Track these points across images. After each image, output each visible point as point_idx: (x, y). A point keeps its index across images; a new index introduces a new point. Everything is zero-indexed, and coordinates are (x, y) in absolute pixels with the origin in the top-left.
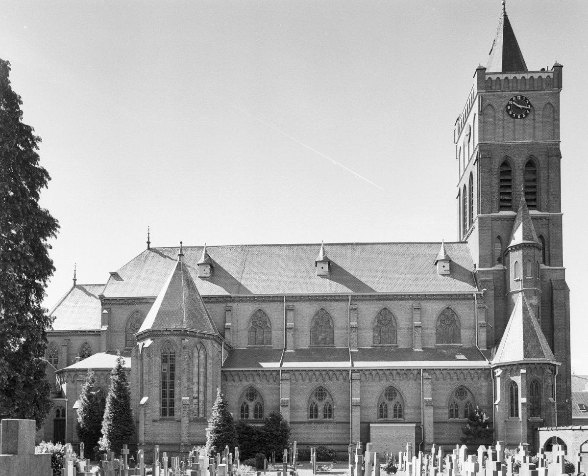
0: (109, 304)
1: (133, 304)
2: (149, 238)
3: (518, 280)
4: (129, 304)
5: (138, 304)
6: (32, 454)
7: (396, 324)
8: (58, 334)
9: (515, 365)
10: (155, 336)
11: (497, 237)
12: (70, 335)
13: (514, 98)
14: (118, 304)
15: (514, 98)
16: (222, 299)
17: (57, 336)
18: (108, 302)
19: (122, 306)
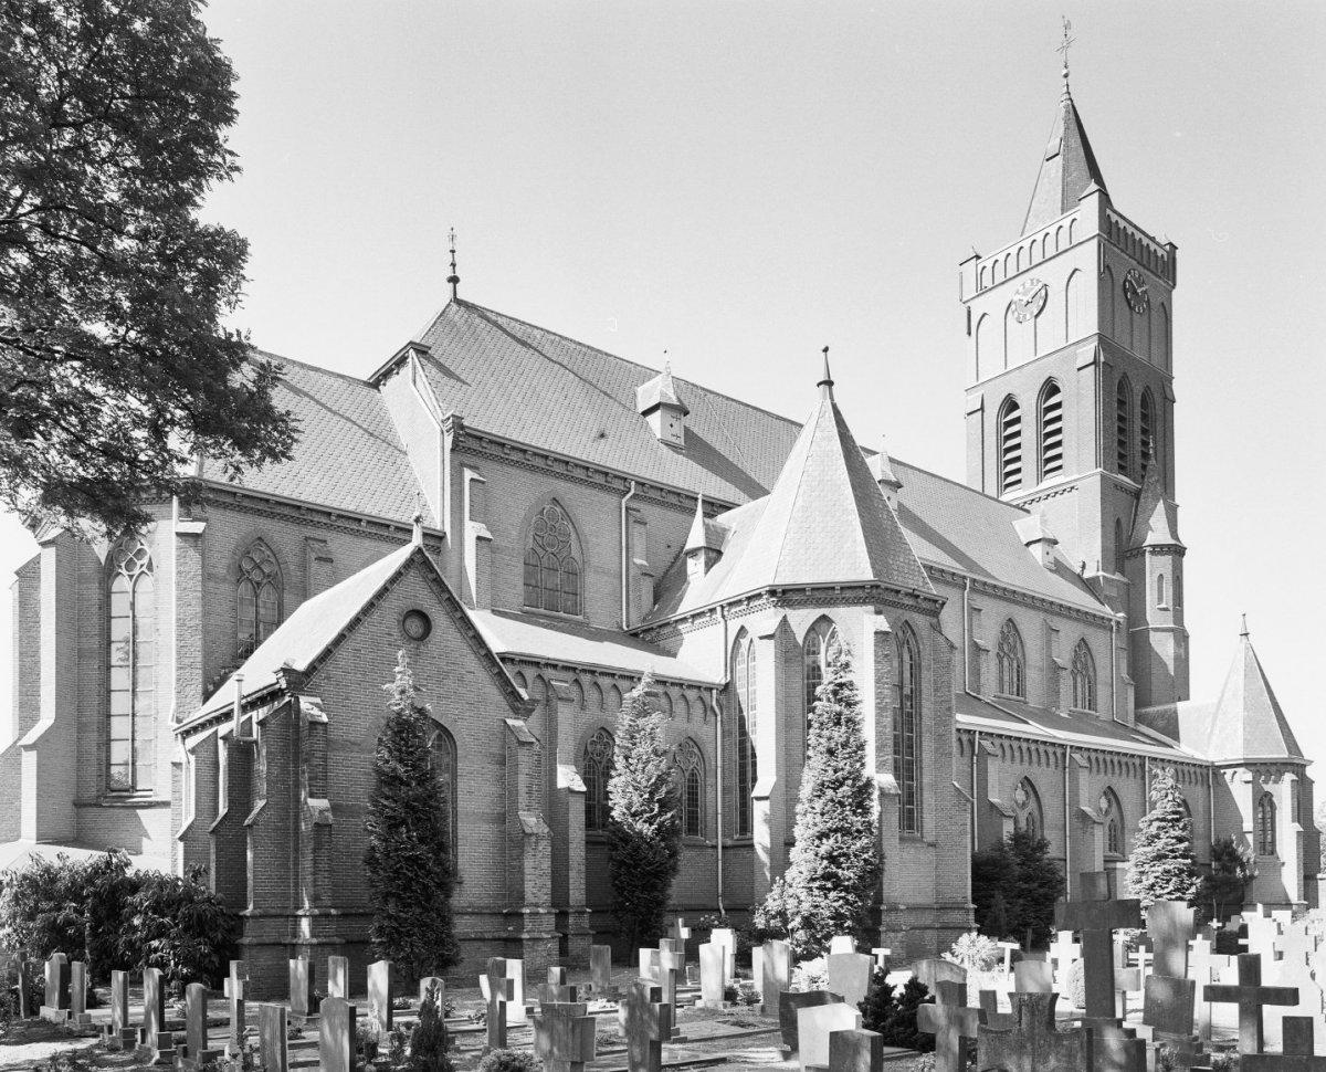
0: (476, 453)
1: (547, 472)
2: (453, 265)
3: (1166, 609)
4: (533, 469)
5: (558, 476)
6: (430, 975)
7: (1024, 655)
8: (286, 511)
9: (1275, 764)
10: (885, 602)
11: (1296, 991)
12: (329, 527)
13: (1021, 289)
14: (503, 461)
15: (1021, 289)
16: (521, 455)
17: (283, 517)
18: (474, 445)
19: (514, 471)
